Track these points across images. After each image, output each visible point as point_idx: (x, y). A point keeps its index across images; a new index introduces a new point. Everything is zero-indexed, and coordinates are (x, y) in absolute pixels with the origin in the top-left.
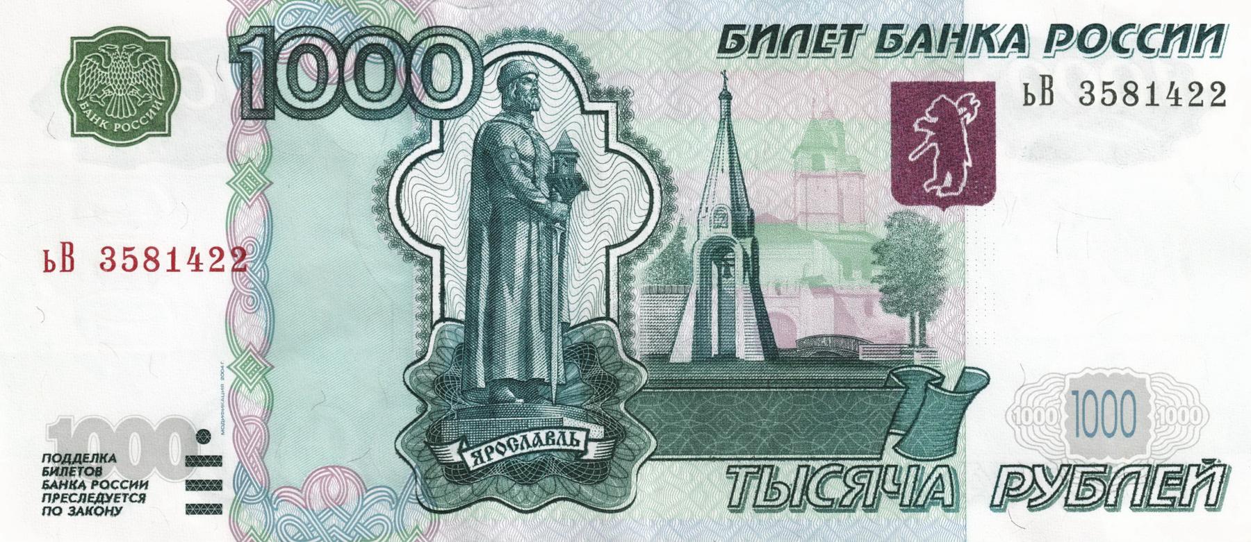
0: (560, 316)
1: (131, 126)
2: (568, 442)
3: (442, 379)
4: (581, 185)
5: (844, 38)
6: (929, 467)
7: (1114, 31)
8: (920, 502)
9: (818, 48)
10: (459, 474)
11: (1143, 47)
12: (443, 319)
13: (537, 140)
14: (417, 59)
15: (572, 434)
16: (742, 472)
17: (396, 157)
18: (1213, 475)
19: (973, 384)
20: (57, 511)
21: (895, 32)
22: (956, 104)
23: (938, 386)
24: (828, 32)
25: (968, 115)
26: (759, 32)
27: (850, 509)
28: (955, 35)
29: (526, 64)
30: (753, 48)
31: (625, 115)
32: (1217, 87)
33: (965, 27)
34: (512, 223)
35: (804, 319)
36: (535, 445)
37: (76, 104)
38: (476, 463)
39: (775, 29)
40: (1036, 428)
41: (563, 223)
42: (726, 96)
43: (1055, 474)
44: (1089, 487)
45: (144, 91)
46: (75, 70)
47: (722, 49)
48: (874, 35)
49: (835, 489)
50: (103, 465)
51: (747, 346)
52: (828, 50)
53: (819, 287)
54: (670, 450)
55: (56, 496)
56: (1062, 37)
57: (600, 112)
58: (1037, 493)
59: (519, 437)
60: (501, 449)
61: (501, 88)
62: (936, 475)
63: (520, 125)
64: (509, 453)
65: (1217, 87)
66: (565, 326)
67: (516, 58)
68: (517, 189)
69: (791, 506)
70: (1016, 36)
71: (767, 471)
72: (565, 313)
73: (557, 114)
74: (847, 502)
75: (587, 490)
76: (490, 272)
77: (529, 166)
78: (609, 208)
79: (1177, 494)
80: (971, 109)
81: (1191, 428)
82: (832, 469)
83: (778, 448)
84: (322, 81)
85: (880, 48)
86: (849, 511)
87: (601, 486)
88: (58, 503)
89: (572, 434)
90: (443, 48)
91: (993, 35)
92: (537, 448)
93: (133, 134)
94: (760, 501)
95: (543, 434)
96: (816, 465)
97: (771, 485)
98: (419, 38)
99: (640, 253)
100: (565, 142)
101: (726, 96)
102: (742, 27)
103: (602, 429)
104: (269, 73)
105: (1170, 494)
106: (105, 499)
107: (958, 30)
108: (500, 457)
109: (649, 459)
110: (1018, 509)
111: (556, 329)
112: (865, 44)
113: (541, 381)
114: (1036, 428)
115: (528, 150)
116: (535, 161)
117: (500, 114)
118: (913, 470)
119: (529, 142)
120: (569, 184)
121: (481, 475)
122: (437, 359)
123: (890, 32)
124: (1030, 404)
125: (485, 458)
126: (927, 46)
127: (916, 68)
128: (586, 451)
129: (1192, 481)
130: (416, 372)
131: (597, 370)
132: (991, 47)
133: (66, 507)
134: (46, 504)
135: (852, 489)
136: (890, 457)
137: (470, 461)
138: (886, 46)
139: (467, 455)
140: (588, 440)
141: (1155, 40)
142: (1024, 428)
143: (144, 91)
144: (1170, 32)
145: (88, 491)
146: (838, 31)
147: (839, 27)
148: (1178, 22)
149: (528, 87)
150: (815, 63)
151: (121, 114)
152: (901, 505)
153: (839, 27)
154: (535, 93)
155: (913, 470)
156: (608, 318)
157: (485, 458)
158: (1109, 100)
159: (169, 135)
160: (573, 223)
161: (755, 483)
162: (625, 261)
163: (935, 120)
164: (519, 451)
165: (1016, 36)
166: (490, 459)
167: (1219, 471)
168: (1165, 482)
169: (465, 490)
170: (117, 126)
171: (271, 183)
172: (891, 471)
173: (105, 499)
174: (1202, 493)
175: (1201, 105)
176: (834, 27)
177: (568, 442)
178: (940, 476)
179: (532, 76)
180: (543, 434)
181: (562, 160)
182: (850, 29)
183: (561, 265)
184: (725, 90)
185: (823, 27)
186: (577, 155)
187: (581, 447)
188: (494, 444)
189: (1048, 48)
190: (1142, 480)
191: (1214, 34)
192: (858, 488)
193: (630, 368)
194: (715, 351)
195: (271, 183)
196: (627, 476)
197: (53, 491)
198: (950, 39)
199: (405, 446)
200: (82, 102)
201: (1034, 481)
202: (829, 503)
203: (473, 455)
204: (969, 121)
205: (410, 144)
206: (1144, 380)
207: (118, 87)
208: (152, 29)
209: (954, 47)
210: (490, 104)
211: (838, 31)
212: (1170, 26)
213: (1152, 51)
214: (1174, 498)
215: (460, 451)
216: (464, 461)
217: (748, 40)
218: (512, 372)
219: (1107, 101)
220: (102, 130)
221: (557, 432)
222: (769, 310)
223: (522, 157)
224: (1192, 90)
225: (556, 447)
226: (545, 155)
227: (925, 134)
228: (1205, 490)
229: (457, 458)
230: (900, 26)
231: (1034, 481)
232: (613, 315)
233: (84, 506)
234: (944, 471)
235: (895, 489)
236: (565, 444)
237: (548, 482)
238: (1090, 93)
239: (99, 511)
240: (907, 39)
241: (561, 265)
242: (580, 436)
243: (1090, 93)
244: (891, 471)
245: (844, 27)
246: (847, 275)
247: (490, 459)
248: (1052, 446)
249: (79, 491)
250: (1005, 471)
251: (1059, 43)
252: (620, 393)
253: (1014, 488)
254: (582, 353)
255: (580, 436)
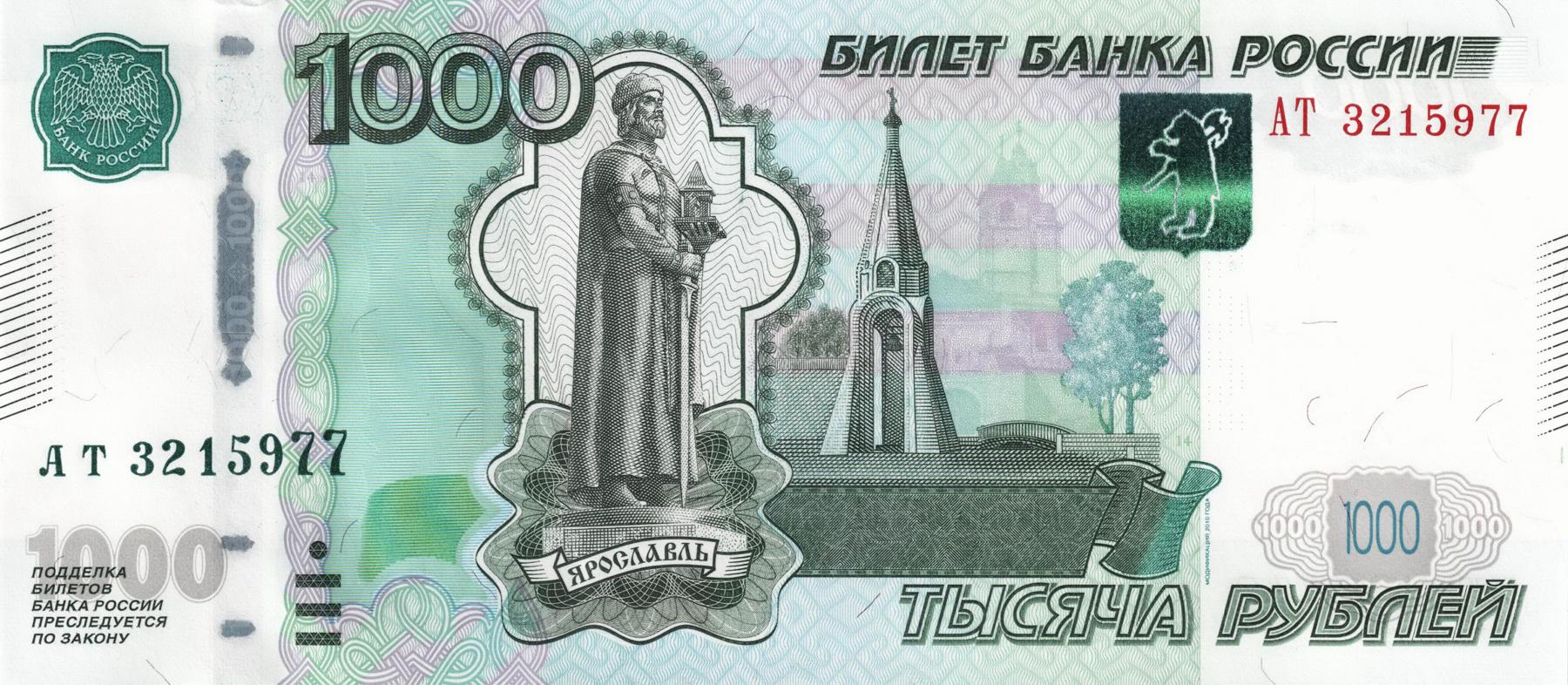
0: (691, 397)
1: (118, 158)
2: (693, 554)
3: (535, 476)
4: (715, 231)
5: (979, 52)
6: (1157, 584)
7: (1318, 45)
8: (1144, 630)
9: (946, 65)
10: (554, 594)
11: (1356, 67)
12: (537, 400)
13: (662, 175)
14: (517, 69)
15: (699, 546)
16: (923, 592)
17: (478, 193)
18: (1501, 599)
19: (1201, 480)
20: (50, 638)
21: (1045, 45)
22: (1202, 123)
23: (1158, 485)
24: (957, 46)
25: (1217, 136)
26: (872, 45)
27: (1055, 639)
28: (1117, 49)
29: (650, 80)
30: (865, 65)
31: (765, 141)
32: (1380, 111)
33: (1129, 39)
34: (630, 277)
35: (984, 402)
36: (649, 560)
37: (50, 130)
38: (574, 583)
39: (891, 41)
40: (1292, 542)
41: (695, 279)
42: (894, 121)
43: (1300, 596)
44: (1343, 612)
45: (134, 113)
46: (49, 87)
47: (827, 64)
48: (1017, 49)
49: (1037, 614)
50: (110, 580)
51: (917, 433)
52: (961, 67)
53: (1007, 361)
54: (817, 564)
55: (49, 620)
56: (1255, 52)
57: (735, 139)
58: (1280, 621)
59: (627, 549)
60: (606, 565)
61: (618, 108)
62: (1402, 592)
63: (641, 157)
64: (615, 570)
65: (1380, 111)
66: (698, 409)
67: (639, 69)
68: (638, 235)
69: (1073, 635)
70: (1077, 49)
71: (954, 592)
72: (697, 389)
73: (686, 144)
74: (1052, 630)
75: (716, 616)
76: (605, 344)
77: (653, 209)
78: (747, 263)
79: (1452, 624)
80: (1220, 129)
81: (1489, 540)
82: (1034, 589)
83: (970, 562)
84: (405, 99)
85: (1025, 65)
86: (1054, 642)
87: (734, 611)
88: (51, 628)
89: (699, 546)
90: (396, 62)
91: (1164, 49)
92: (654, 563)
93: (119, 168)
94: (944, 629)
95: (660, 546)
96: (1018, 582)
97: (960, 606)
98: (518, 46)
99: (782, 316)
100: (698, 178)
101: (894, 121)
102: (853, 38)
103: (744, 538)
104: (342, 87)
105: (1445, 624)
106: (113, 622)
107: (1121, 43)
108: (605, 575)
109: (794, 575)
110: (1252, 642)
111: (686, 413)
112: (1008, 59)
113: (667, 479)
114: (1292, 542)
115: (650, 186)
116: (659, 200)
117: (618, 143)
118: (1135, 592)
119: (652, 175)
120: (703, 232)
121: (584, 597)
122: (529, 452)
123: (1037, 46)
124: (1284, 512)
125: (586, 576)
126: (1082, 63)
127: (1155, 83)
128: (713, 569)
129: (1473, 609)
130: (502, 467)
131: (726, 468)
132: (1162, 66)
133: (59, 632)
134: (37, 630)
135: (1056, 615)
136: (1096, 574)
137: (568, 579)
138: (834, 62)
139: (564, 571)
140: (716, 552)
141: (1371, 57)
142: (1276, 543)
143: (134, 113)
144: (1390, 46)
145: (89, 614)
146: (972, 44)
147: (973, 39)
148: (1400, 33)
149: (650, 108)
150: (941, 84)
151: (106, 142)
152: (1119, 634)
153: (973, 39)
154: (659, 115)
155: (1135, 592)
156: (743, 401)
157: (586, 576)
158: (1436, 128)
159: (166, 168)
160: (706, 276)
161: (938, 607)
162: (763, 327)
163: (1175, 142)
164: (629, 568)
165: (1077, 49)
166: (591, 577)
167: (1509, 593)
168: (1439, 608)
169: (565, 616)
170: (100, 159)
171: (279, 229)
172: (1107, 592)
173: (113, 622)
174: (1488, 624)
175: (1388, 133)
176: (967, 39)
177: (693, 554)
178: (1169, 598)
179: (655, 95)
180: (660, 546)
181: (692, 201)
182: (988, 41)
183: (691, 336)
184: (892, 110)
185: (953, 40)
186: (712, 193)
187: (709, 563)
188: (597, 558)
189: (1237, 66)
190: (1411, 603)
191: (1481, 49)
192: (1065, 613)
193: (771, 463)
194: (878, 440)
195: (279, 229)
196: (766, 599)
197: (46, 614)
198: (1110, 54)
199: (489, 561)
200: (57, 127)
201: (1274, 606)
202: (1030, 631)
203: (570, 571)
204: (1218, 144)
205: (496, 178)
206: (1428, 482)
207: (107, 105)
208: (145, 35)
209: (1116, 62)
210: (602, 129)
211: (972, 44)
212: (1390, 39)
213: (1366, 69)
214: (1451, 629)
215: (556, 567)
216: (561, 579)
217: (860, 52)
218: (632, 469)
219: (1350, 130)
220: (81, 164)
221: (679, 544)
222: (946, 387)
223: (643, 196)
224: (1376, 115)
225: (677, 562)
226: (672, 192)
227: (1163, 159)
228: (1491, 620)
229: (553, 576)
230: (1049, 39)
231: (1274, 606)
232: (750, 397)
233: (83, 631)
234: (1174, 593)
235: (1112, 614)
236: (689, 558)
237: (666, 606)
238: (1356, 119)
239: (100, 638)
240: (1058, 54)
241: (691, 336)
242: (708, 548)
243: (1356, 119)
244: (1107, 592)
245: (979, 39)
246: (1041, 346)
247: (591, 577)
248: (1306, 564)
249: (78, 614)
250: (1239, 592)
251: (1250, 59)
252: (759, 494)
253: (1257, 612)
254: (714, 446)
255: (708, 548)
